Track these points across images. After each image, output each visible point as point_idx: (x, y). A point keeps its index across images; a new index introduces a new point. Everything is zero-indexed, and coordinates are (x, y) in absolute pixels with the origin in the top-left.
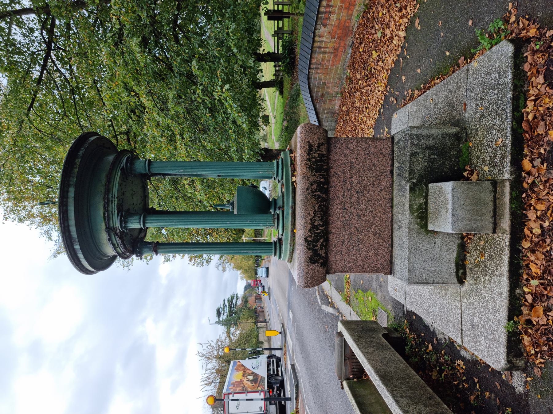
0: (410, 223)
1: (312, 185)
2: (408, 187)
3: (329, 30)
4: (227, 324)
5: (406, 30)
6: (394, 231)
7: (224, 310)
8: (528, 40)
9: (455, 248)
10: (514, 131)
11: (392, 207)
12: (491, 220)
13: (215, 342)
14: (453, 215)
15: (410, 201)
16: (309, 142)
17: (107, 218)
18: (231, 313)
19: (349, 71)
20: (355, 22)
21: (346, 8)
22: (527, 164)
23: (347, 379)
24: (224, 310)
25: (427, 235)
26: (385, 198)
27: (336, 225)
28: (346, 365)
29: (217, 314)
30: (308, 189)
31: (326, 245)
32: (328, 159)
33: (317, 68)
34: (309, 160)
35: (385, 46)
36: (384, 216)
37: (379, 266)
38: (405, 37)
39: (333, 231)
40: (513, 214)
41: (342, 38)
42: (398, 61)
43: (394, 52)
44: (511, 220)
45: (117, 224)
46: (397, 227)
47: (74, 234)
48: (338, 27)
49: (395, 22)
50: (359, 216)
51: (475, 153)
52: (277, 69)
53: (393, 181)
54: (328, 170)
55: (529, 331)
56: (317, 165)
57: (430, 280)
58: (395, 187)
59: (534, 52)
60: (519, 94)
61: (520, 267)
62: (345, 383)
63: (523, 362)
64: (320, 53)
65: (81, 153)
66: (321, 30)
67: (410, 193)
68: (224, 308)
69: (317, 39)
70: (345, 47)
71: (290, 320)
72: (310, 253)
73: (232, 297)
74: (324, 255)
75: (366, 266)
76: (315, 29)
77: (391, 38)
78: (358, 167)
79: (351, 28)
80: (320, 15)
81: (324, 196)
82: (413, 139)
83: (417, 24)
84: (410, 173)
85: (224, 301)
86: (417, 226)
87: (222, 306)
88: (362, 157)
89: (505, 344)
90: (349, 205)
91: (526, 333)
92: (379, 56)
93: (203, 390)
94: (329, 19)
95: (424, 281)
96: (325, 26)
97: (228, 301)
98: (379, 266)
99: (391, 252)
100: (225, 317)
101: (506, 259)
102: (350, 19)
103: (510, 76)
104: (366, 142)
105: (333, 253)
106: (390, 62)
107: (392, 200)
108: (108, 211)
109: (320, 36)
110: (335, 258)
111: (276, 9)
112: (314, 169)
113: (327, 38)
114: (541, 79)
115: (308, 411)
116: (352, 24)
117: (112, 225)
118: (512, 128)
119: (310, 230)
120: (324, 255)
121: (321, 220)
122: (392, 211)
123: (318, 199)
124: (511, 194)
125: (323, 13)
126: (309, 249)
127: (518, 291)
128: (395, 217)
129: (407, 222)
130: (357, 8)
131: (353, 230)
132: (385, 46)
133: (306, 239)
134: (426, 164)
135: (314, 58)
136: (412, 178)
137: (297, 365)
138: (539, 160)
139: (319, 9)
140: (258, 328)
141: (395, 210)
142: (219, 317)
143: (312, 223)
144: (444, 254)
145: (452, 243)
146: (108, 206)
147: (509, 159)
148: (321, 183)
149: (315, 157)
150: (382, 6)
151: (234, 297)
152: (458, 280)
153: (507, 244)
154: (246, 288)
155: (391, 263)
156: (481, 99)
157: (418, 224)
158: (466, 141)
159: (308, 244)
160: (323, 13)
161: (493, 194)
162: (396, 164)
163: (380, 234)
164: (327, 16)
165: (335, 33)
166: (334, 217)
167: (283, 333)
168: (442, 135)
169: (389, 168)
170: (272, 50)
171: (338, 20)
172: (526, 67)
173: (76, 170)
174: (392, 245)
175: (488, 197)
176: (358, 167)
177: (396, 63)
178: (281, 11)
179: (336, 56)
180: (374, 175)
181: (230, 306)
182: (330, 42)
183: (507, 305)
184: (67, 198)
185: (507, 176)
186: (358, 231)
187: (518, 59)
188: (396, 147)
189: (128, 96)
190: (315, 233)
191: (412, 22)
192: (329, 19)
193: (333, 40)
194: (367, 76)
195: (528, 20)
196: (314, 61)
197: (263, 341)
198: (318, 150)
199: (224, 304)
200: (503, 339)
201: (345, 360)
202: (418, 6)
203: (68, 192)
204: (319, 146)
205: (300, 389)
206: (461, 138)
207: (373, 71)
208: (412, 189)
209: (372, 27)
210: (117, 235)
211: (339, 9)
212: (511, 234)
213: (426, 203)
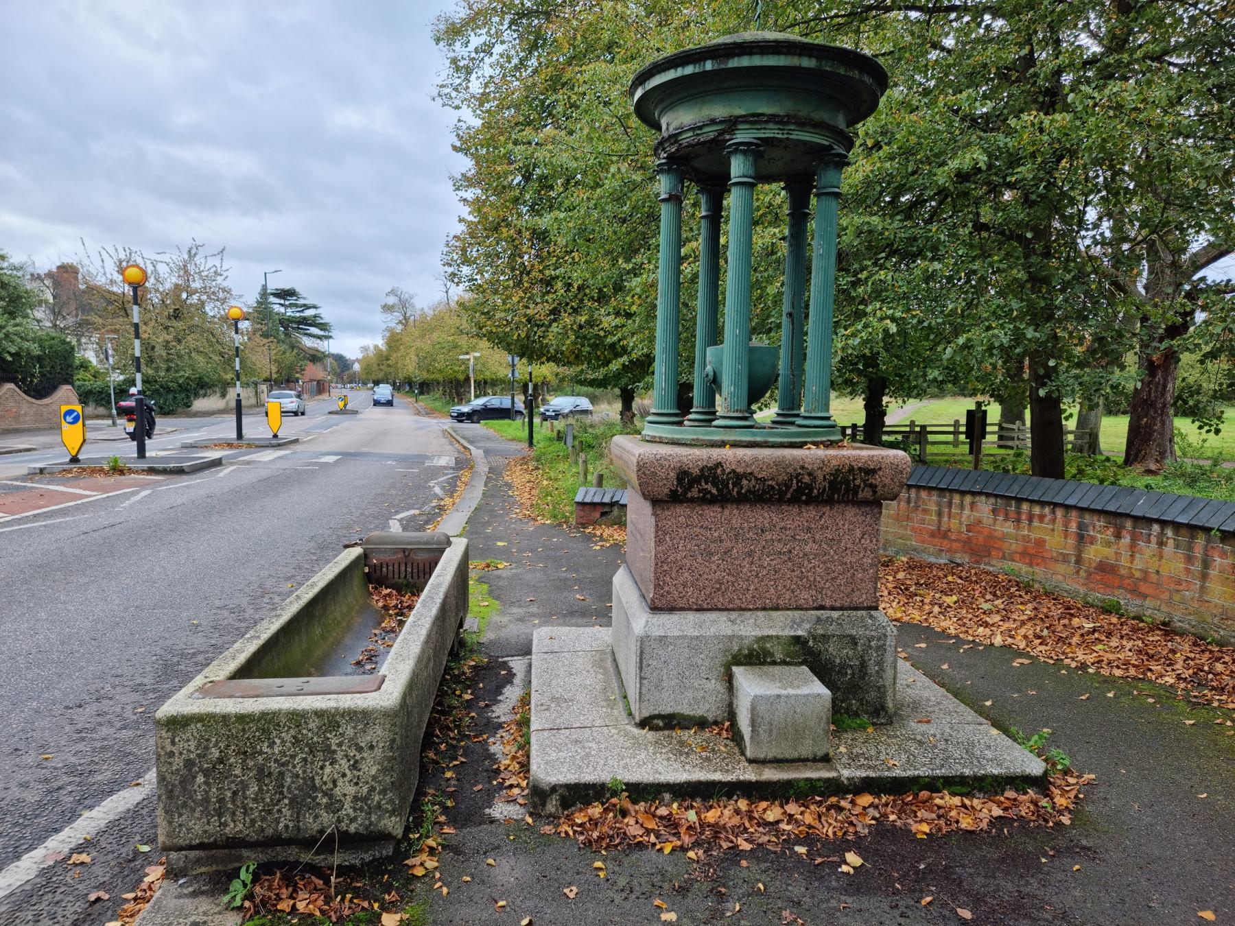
0: (741, 638)
1: (810, 474)
2: (800, 633)
3: (985, 521)
4: (262, 312)
5: (1006, 648)
6: (725, 613)
7: (291, 305)
8: (1048, 795)
9: (699, 713)
10: (915, 780)
11: (764, 609)
12: (770, 756)
13: (224, 284)
14: (779, 696)
15: (778, 637)
16: (880, 469)
17: (754, 120)
18: (285, 322)
19: (905, 559)
20: (997, 565)
21: (1026, 548)
22: (865, 800)
23: (365, 556)
24: (291, 305)
25: (722, 665)
26: (779, 598)
27: (736, 517)
28: (395, 551)
29: (283, 291)
30: (803, 468)
31: (706, 500)
32: (847, 503)
33: (909, 501)
34: (851, 469)
35: (970, 616)
36: (749, 597)
37: (666, 588)
38: (992, 644)
39: (727, 512)
40: (789, 784)
41: (968, 546)
42: (949, 637)
43: (964, 629)
44: (778, 781)
45: (742, 136)
46: (732, 617)
47: (734, 63)
48: (991, 537)
49: (1016, 629)
50: (750, 554)
51: (860, 736)
52: (849, 431)
53: (807, 609)
54: (830, 502)
55: (611, 815)
56: (841, 483)
57: (647, 672)
58: (797, 614)
59: (1035, 803)
60: (969, 785)
61: (705, 799)
62: (358, 551)
63: (553, 810)
64: (939, 505)
65: (855, 74)
66: (985, 507)
67: (792, 637)
68: (296, 305)
69: (968, 499)
70: (950, 550)
71: (317, 457)
72: (696, 471)
73: (323, 327)
74: (689, 495)
75: (666, 568)
76: (988, 495)
77: (986, 625)
78: (832, 552)
79: (986, 560)
80: (1013, 502)
81: (789, 496)
82: (879, 639)
83: (1021, 661)
84: (824, 636)
85: (315, 307)
86: (736, 648)
87: (301, 302)
88: (848, 559)
89: (582, 781)
90: (769, 537)
91: (606, 810)
92: (949, 607)
93: (104, 253)
94: (1007, 519)
95: (645, 663)
96: (994, 511)
97: (315, 316)
98: (666, 588)
99: (690, 609)
100: (277, 308)
101: (717, 776)
102: (1004, 558)
103: (996, 772)
104: (871, 565)
105: (688, 511)
106: (943, 624)
107: (777, 609)
108: (767, 122)
109: (973, 504)
110: (681, 513)
111: (989, 429)
112: (835, 479)
113: (969, 517)
114: (997, 812)
115: (138, 497)
116: (994, 562)
117: (740, 127)
118: (919, 777)
119: (734, 471)
120: (689, 495)
121: (749, 491)
122: (757, 609)
123: (786, 485)
124: (819, 780)
125: (1018, 507)
126: (702, 470)
127: (667, 796)
128: (748, 614)
129: (743, 633)
130: (1025, 569)
131: (729, 544)
132: (970, 616)
133: (719, 464)
134: (838, 661)
135: (929, 495)
136: (814, 639)
137: (224, 472)
138: (878, 816)
139: (1026, 500)
140: (256, 384)
141: (761, 614)
142: (276, 295)
143: (745, 476)
144: (689, 694)
145: (707, 706)
146: (776, 123)
147: (872, 774)
148: (811, 491)
149: (854, 479)
150: (1035, 609)
151: (324, 330)
152: (646, 719)
153: (741, 778)
154: (339, 359)
155: (672, 609)
156: (946, 740)
157: (740, 650)
158: (874, 724)
159: (710, 469)
160: (1018, 507)
161: (811, 757)
162: (835, 614)
163: (719, 590)
164: (1012, 515)
165: (979, 532)
166: (749, 513)
167: (275, 442)
168: (884, 686)
169: (828, 603)
170: (888, 420)
171: (1005, 536)
172: (1010, 794)
173: (842, 71)
174: (700, 609)
175: (806, 750)
176: (832, 552)
177: (944, 634)
178: (983, 434)
179: (932, 535)
180: (818, 579)
181: (305, 321)
182: (961, 523)
183: (645, 781)
184: (800, 55)
185: (846, 773)
186: (725, 553)
187: (1022, 782)
188: (864, 613)
189: (867, 134)
190: (728, 480)
191: (1020, 654)
192: (1007, 519)
193: (964, 529)
194: (907, 589)
195: (1076, 797)
196: (924, 494)
197: (228, 397)
198: (866, 485)
199: (307, 307)
200: (589, 777)
201: (404, 550)
202: (1052, 662)
203: (810, 56)
204: (873, 487)
205: (176, 478)
206: (878, 717)
207: (918, 598)
208: (797, 640)
209: (995, 595)
210: (720, 134)
211: (1024, 536)
212: (757, 782)
213: (774, 663)
